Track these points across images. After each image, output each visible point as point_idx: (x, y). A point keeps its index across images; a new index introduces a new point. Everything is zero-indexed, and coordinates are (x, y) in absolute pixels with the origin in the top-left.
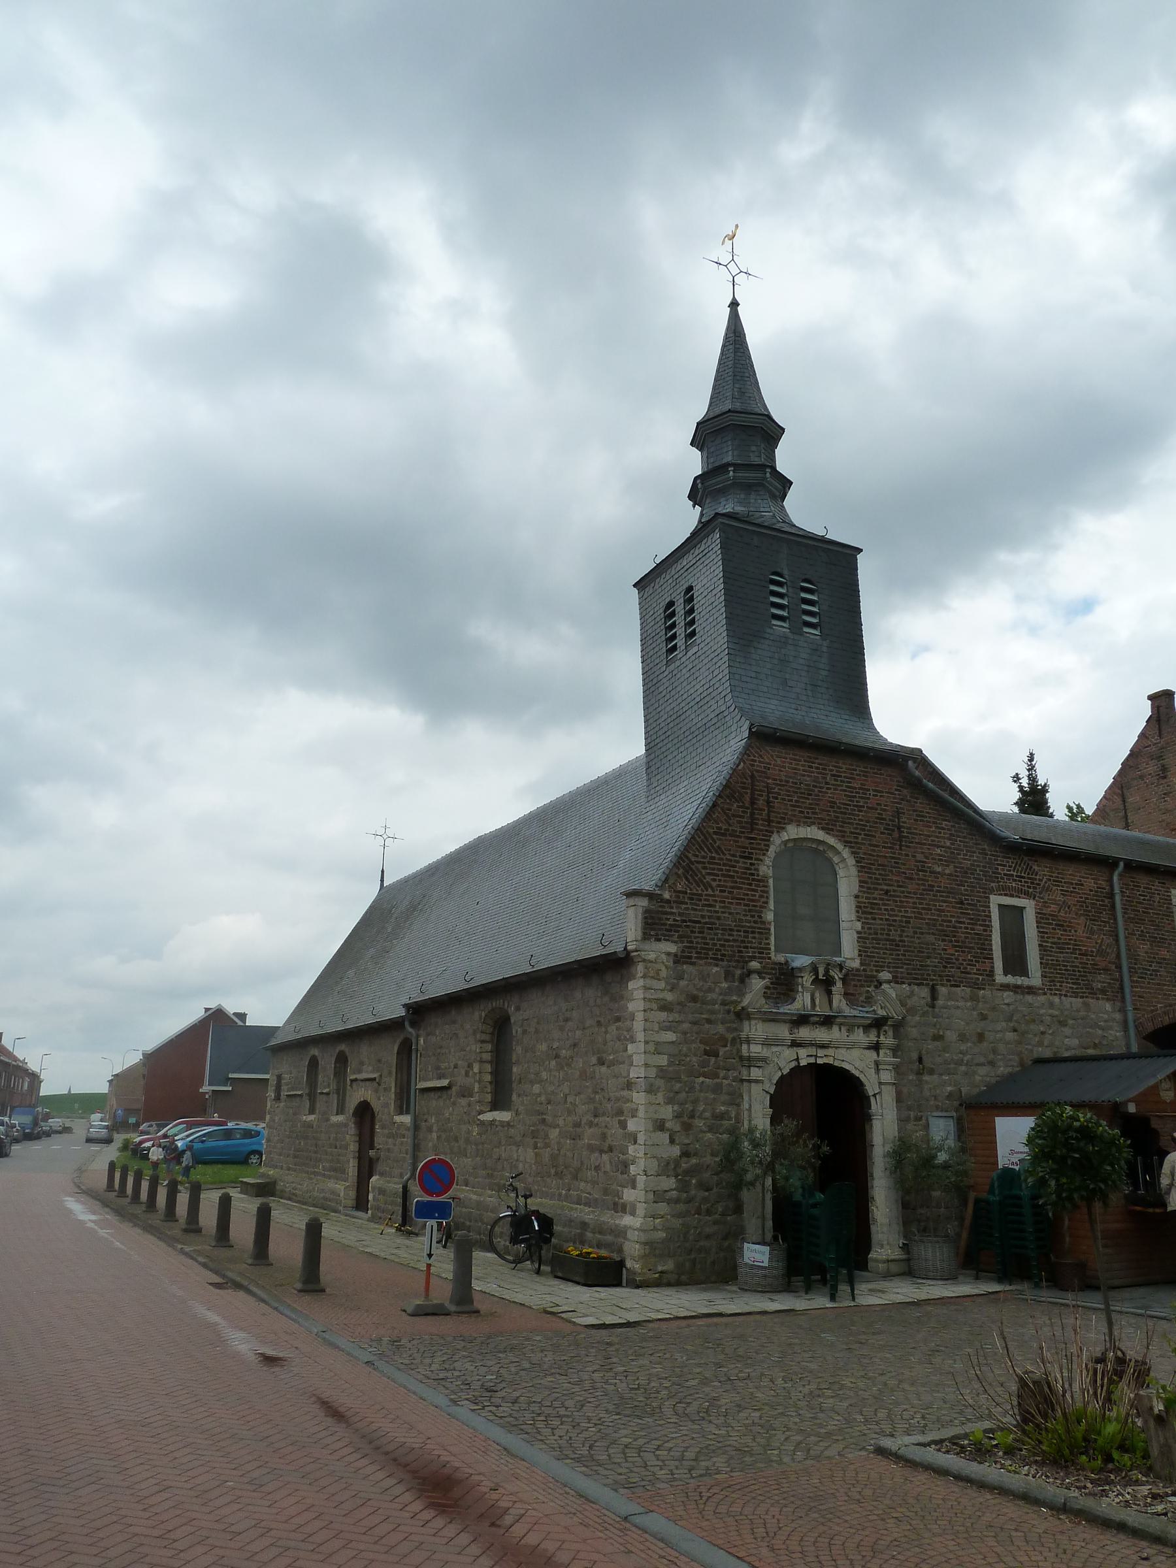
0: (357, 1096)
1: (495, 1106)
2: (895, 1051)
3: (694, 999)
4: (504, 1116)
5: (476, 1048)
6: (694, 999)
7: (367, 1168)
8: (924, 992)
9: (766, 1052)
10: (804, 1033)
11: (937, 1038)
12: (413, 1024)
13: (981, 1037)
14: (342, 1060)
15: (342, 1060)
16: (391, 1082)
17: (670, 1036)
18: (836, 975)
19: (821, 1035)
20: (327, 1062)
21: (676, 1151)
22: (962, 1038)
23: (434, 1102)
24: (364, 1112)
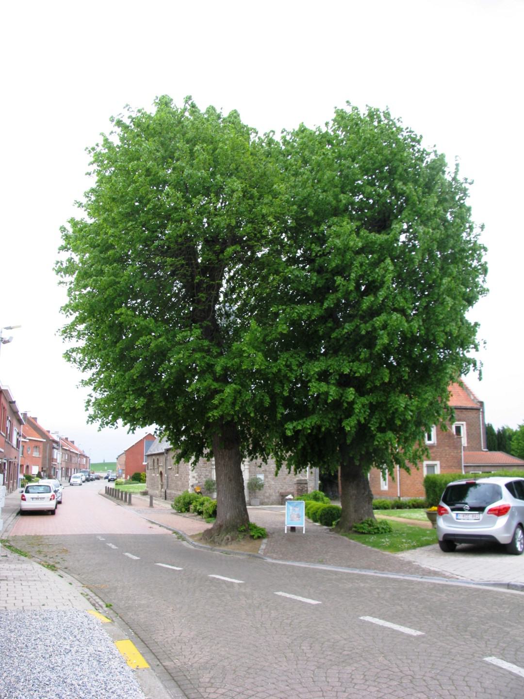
0: (161, 469)
4: (177, 475)
12: (166, 453)
14: (158, 460)
15: (158, 460)
20: (156, 461)
21: (197, 482)
24: (161, 473)
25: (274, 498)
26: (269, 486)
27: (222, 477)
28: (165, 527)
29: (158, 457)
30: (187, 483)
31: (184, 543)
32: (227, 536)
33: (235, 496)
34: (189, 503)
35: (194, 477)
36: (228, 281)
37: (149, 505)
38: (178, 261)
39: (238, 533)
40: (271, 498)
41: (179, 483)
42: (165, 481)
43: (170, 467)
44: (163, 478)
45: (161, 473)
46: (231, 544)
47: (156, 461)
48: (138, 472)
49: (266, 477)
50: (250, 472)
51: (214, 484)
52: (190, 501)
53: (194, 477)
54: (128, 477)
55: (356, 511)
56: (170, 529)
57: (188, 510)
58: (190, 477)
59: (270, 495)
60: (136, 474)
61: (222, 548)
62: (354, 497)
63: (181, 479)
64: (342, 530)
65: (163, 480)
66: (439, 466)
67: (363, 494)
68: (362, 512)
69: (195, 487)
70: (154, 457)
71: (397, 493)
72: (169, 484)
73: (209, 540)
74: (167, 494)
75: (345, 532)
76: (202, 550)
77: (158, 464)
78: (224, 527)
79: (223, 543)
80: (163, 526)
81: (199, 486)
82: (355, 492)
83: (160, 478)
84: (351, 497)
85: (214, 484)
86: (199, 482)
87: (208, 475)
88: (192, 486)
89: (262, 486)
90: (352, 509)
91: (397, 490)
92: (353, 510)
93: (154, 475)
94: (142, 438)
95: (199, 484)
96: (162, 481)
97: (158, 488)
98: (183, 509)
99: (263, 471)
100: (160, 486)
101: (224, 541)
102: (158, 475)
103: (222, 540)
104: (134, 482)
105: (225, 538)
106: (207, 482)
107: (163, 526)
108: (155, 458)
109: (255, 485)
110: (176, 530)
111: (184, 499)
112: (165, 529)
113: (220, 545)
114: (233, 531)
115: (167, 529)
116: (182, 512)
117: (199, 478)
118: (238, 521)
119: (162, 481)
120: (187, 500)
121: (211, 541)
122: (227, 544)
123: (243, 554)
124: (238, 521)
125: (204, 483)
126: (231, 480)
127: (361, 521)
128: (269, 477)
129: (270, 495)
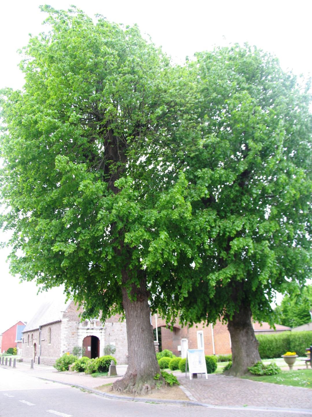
0: (34, 342)
1: (50, 343)
2: (105, 333)
3: (71, 327)
4: (50, 344)
5: (47, 333)
6: (71, 327)
7: (35, 354)
8: (111, 324)
9: (82, 334)
10: (88, 331)
11: (113, 331)
12: (41, 329)
13: (121, 330)
14: (32, 335)
15: (32, 335)
16: (38, 339)
17: (67, 332)
18: (94, 322)
19: (92, 331)
20: (30, 336)
21: (67, 348)
22: (118, 330)
23: (43, 342)
24: (35, 345)
25: (123, 359)
26: (119, 351)
27: (135, 328)
28: (60, 383)
29: (32, 333)
30: (59, 350)
31: (93, 395)
32: (146, 385)
33: (148, 345)
34: (69, 363)
35: (64, 345)
36: (144, 187)
37: (30, 368)
38: (107, 176)
39: (154, 381)
40: (121, 360)
41: (52, 350)
42: (38, 350)
43: (44, 339)
44: (37, 348)
45: (35, 345)
46: (152, 393)
47: (30, 336)
48: (11, 347)
49: (117, 344)
50: (105, 340)
51: (80, 350)
52: (69, 361)
53: (64, 345)
54: (4, 352)
55: (248, 356)
56: (66, 384)
57: (67, 369)
58: (62, 345)
59: (119, 358)
60: (10, 349)
61: (147, 397)
62: (245, 343)
63: (53, 347)
64: (238, 374)
65: (37, 350)
66: (167, 350)
67: (252, 340)
68: (253, 356)
69: (65, 352)
70: (29, 333)
71: (213, 352)
72: (42, 352)
73: (125, 391)
74: (40, 360)
75: (241, 375)
76: (121, 400)
77: (32, 338)
78: (139, 376)
79: (143, 392)
80: (56, 382)
81: (69, 352)
82: (245, 339)
83: (34, 348)
84: (242, 343)
85: (80, 350)
86: (68, 349)
87: (75, 343)
88: (63, 352)
89: (115, 350)
90: (244, 354)
91: (212, 350)
92: (246, 355)
93: (28, 346)
94: (14, 324)
95: (68, 350)
96: (35, 350)
97: (32, 356)
98: (64, 368)
99: (115, 340)
100: (34, 354)
101: (143, 390)
102: (32, 346)
103: (141, 390)
104: (9, 354)
105: (144, 387)
106: (75, 348)
107: (56, 382)
108: (30, 334)
109: (110, 350)
110: (74, 384)
111: (64, 360)
112: (61, 384)
113: (140, 394)
114: (150, 379)
115: (62, 383)
116: (62, 370)
117: (69, 345)
118: (153, 369)
119: (35, 350)
120: (67, 361)
121: (127, 391)
122: (147, 393)
123: (175, 402)
124: (153, 369)
125: (72, 350)
126: (143, 331)
127: (254, 365)
128: (119, 344)
129: (119, 358)
